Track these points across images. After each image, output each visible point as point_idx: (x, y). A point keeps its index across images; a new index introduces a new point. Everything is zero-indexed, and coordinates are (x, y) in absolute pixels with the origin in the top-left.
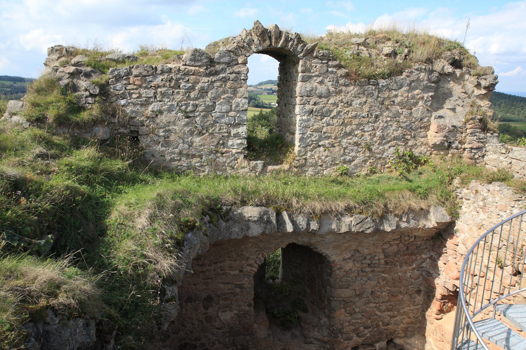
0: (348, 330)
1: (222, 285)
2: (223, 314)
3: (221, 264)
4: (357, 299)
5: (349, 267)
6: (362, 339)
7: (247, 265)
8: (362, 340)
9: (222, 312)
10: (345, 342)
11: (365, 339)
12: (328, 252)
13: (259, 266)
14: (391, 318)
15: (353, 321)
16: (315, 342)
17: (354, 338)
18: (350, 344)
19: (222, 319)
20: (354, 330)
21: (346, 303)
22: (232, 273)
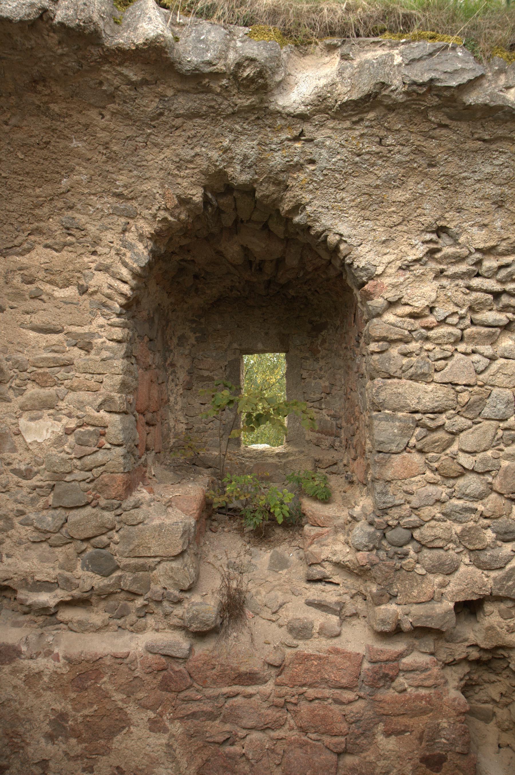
0: (439, 532)
1: (32, 334)
2: (32, 424)
3: (24, 260)
4: (461, 422)
5: (423, 297)
6: (494, 574)
7: (98, 269)
8: (494, 579)
9: (32, 419)
10: (430, 577)
11: (503, 579)
12: (343, 228)
13: (135, 275)
14: (339, 754)
15: (455, 502)
16: (336, 579)
17: (462, 569)
18: (449, 589)
19: (29, 441)
20: (461, 536)
21: (436, 312)
22: (60, 293)
